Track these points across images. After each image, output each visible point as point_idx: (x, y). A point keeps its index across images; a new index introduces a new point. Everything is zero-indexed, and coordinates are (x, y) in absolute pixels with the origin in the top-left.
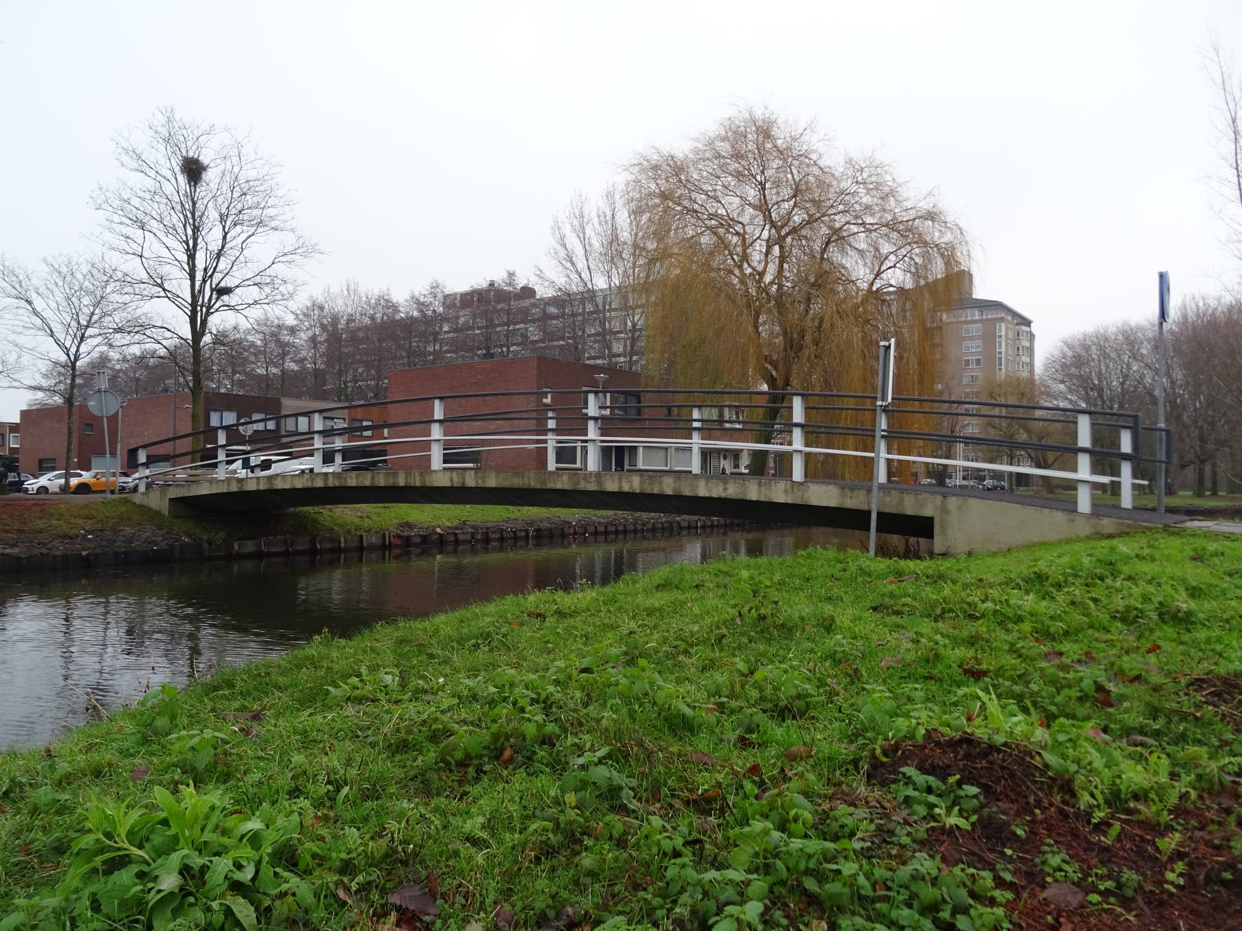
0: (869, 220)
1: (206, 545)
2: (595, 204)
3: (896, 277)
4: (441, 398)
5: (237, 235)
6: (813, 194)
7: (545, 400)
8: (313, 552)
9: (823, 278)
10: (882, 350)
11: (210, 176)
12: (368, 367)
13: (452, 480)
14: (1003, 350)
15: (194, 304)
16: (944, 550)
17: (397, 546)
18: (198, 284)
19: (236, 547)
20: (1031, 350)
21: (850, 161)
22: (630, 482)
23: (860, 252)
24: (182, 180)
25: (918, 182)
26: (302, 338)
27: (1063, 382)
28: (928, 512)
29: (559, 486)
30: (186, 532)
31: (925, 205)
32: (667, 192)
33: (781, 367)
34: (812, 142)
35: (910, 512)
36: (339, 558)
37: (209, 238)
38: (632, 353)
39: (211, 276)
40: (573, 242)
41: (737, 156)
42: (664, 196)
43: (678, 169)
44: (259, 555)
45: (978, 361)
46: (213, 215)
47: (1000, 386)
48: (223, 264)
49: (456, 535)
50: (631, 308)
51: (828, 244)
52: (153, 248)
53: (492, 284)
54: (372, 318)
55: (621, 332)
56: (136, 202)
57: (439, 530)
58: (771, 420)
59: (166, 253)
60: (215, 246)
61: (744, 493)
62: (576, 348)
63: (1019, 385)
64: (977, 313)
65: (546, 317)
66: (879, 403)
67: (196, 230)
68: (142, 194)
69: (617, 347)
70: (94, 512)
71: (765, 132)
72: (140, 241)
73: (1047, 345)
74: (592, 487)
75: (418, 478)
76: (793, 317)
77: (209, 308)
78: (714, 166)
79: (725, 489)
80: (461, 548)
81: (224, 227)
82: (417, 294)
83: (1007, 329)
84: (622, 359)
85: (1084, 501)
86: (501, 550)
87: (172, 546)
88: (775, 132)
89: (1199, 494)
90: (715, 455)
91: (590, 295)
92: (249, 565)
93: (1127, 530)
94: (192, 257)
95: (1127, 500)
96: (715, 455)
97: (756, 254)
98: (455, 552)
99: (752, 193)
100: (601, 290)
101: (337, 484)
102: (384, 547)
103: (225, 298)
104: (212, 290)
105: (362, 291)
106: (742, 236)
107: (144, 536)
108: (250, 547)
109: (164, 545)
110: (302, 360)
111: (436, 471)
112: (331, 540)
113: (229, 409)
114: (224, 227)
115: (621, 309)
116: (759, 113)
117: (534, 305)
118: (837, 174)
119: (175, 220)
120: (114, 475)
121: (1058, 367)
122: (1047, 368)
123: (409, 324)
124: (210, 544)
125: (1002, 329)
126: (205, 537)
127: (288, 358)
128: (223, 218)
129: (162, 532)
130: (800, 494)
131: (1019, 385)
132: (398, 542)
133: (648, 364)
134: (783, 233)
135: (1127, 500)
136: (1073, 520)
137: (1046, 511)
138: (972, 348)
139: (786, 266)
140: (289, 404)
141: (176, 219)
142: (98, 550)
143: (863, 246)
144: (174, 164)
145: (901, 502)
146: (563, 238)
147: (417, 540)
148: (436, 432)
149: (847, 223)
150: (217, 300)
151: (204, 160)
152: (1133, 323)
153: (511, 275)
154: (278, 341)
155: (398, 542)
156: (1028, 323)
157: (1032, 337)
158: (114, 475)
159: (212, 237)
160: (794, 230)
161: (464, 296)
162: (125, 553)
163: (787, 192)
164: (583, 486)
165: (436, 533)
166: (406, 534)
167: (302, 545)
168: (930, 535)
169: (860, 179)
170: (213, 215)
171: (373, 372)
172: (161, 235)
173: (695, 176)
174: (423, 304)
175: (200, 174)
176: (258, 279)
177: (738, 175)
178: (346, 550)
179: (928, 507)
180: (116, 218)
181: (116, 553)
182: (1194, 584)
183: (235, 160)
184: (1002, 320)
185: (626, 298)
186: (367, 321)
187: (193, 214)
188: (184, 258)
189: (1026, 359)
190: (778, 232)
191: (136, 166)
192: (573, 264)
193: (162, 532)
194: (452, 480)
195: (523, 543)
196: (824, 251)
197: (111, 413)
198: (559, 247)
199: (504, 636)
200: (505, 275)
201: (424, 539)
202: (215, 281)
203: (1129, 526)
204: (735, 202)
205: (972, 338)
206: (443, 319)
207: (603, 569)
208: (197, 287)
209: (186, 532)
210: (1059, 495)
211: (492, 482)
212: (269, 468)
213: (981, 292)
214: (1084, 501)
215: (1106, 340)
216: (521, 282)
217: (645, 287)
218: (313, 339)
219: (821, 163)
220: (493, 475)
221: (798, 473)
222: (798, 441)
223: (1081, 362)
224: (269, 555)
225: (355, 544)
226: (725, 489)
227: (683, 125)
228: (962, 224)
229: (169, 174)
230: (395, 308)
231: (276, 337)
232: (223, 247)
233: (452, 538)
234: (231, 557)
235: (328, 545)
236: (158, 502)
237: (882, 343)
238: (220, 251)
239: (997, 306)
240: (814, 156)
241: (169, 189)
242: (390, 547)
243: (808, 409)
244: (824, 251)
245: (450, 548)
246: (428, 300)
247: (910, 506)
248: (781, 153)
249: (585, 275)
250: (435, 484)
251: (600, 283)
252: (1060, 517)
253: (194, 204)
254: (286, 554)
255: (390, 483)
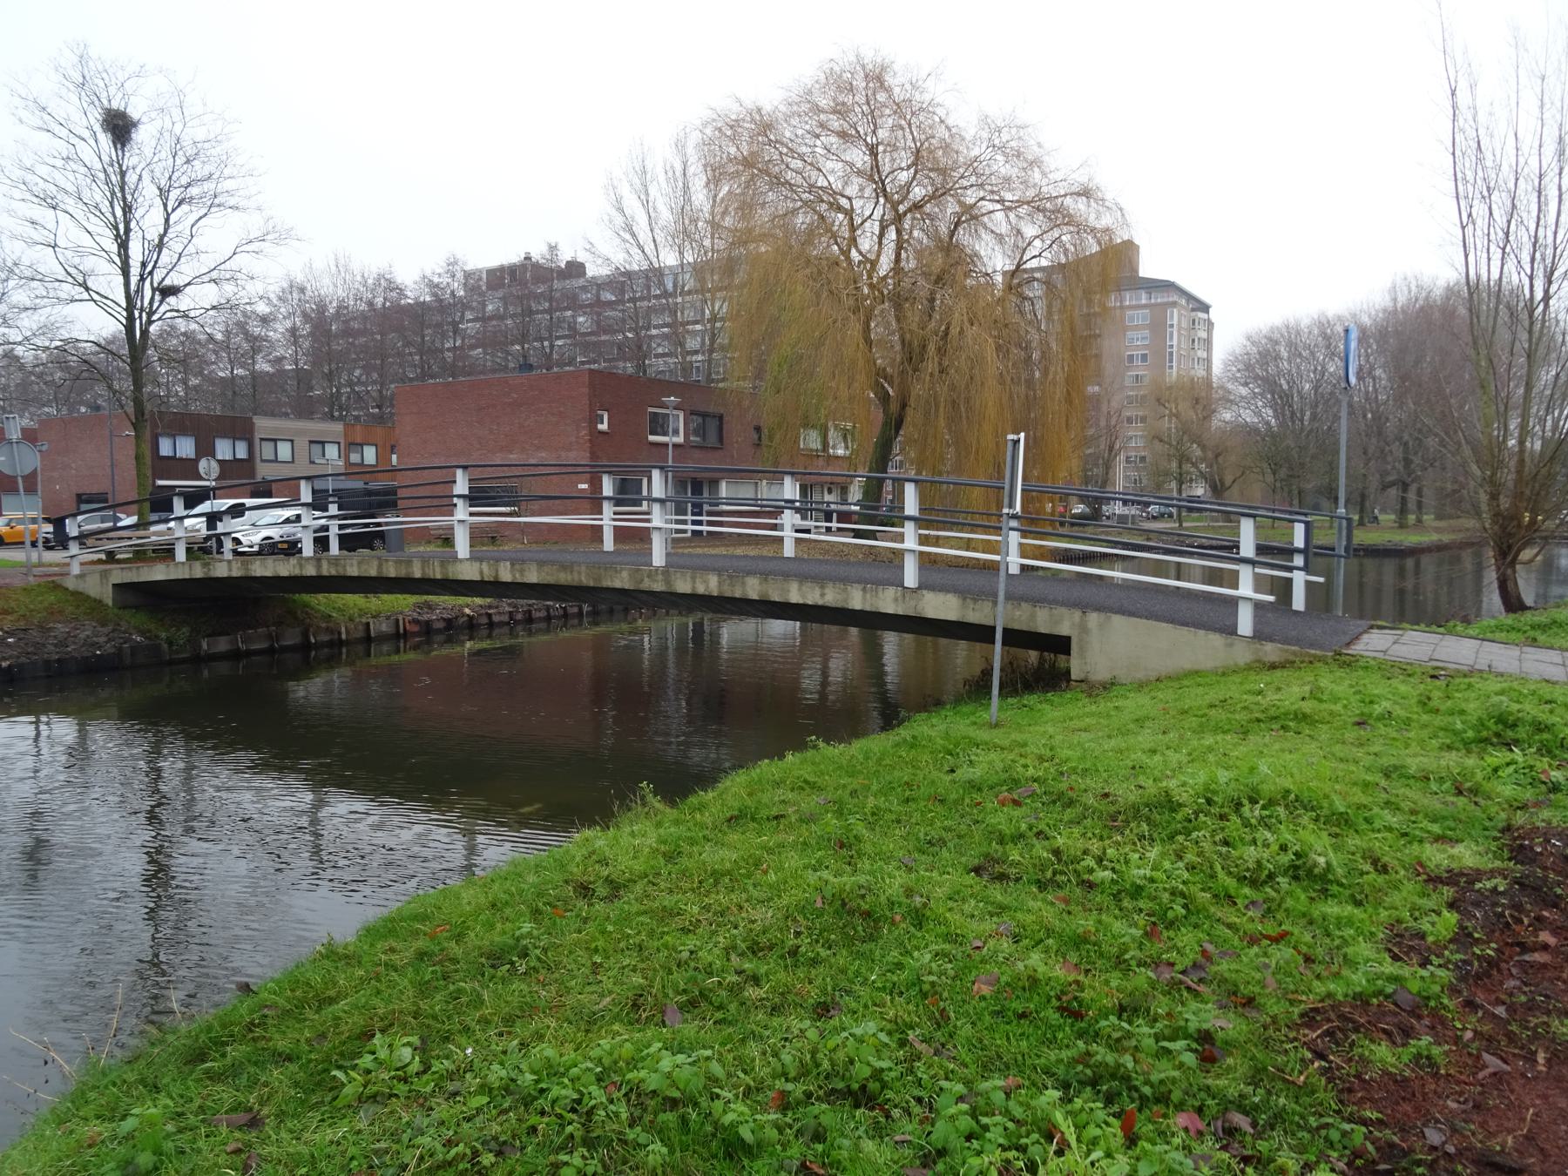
0: (1008, 196)
1: (165, 646)
2: (662, 157)
3: (1040, 258)
4: (465, 468)
5: (183, 217)
6: (935, 161)
7: (600, 427)
8: (305, 647)
9: (950, 262)
10: (1010, 445)
11: (140, 136)
12: (367, 369)
13: (481, 573)
14: (1175, 343)
15: (130, 308)
16: (1082, 676)
17: (415, 634)
18: (134, 280)
19: (205, 646)
20: (1208, 343)
21: (985, 120)
22: (706, 582)
23: (1000, 238)
24: (105, 140)
25: (1066, 159)
26: (277, 332)
27: (1246, 384)
28: (1064, 629)
29: (618, 584)
30: (136, 630)
31: (1081, 178)
32: (749, 158)
33: (896, 381)
34: (934, 91)
35: (1042, 630)
36: (340, 653)
37: (145, 224)
38: (711, 351)
39: (151, 273)
40: (633, 206)
41: (840, 110)
42: (748, 162)
43: (765, 127)
44: (235, 655)
45: (1144, 357)
46: (149, 191)
47: (1170, 388)
48: (166, 258)
49: (489, 616)
50: (709, 291)
51: (957, 225)
52: (70, 234)
53: (528, 258)
54: (370, 304)
55: (696, 322)
56: (43, 170)
57: (467, 611)
58: (879, 512)
59: (87, 241)
60: (153, 235)
61: (846, 600)
62: (640, 347)
63: (1193, 388)
64: (1144, 296)
65: (599, 303)
66: (1005, 511)
67: (127, 209)
68: (52, 161)
69: (692, 343)
70: (13, 604)
71: (877, 78)
72: (51, 226)
73: (1231, 334)
74: (658, 587)
75: (438, 569)
76: (913, 316)
77: (151, 313)
78: (812, 124)
79: (823, 595)
80: (496, 631)
81: (165, 205)
82: (428, 273)
83: (1180, 315)
84: (700, 358)
85: (1245, 622)
86: (548, 631)
87: (120, 649)
88: (889, 80)
89: (1402, 525)
90: (818, 488)
91: (654, 274)
92: (223, 668)
93: (1292, 658)
94: (123, 245)
95: (1299, 602)
96: (818, 488)
97: (866, 243)
98: (490, 636)
99: (859, 157)
100: (670, 268)
101: (333, 573)
102: (398, 637)
103: (172, 300)
104: (154, 290)
105: (356, 267)
106: (849, 213)
107: (82, 636)
108: (223, 645)
109: (109, 648)
110: (280, 360)
111: (461, 561)
112: (329, 630)
113: (184, 432)
114: (165, 205)
115: (697, 292)
116: (868, 57)
117: (583, 288)
118: (968, 137)
119: (98, 197)
120: (34, 521)
121: (1241, 366)
122: (1227, 365)
123: (418, 312)
124: (170, 644)
125: (1175, 317)
126: (163, 635)
127: (259, 358)
128: (163, 193)
129: (105, 630)
130: (913, 603)
131: (1193, 388)
132: (416, 628)
133: (734, 379)
134: (901, 208)
135: (1299, 602)
136: (1231, 645)
137: (1202, 632)
138: (1138, 340)
139: (903, 255)
140: (263, 425)
141: (99, 196)
142: (23, 660)
143: (1003, 229)
144: (93, 121)
145: (1033, 616)
146: (619, 200)
147: (441, 625)
148: (462, 512)
149: (982, 199)
150: (161, 302)
151: (134, 114)
152: (1331, 314)
153: (553, 248)
154: (246, 333)
155: (416, 628)
156: (1205, 308)
157: (1210, 325)
158: (34, 521)
159: (149, 220)
160: (917, 206)
161: (490, 272)
162: (59, 661)
163: (905, 158)
164: (647, 585)
165: (464, 615)
166: (426, 617)
167: (291, 638)
168: (1067, 652)
169: (997, 142)
170: (149, 191)
171: (375, 376)
172: (79, 215)
173: (788, 134)
174: (437, 286)
175: (129, 132)
176: (214, 275)
177: (842, 135)
178: (347, 643)
179: (1062, 623)
180: (17, 194)
181: (47, 662)
182: (1342, 809)
183: (176, 113)
184: (1174, 304)
185: (702, 281)
186: (363, 307)
187: (122, 190)
188: (114, 248)
189: (1202, 354)
190: (895, 207)
191: (40, 123)
192: (633, 235)
193: (105, 630)
194: (481, 573)
195: (576, 621)
196: (952, 234)
197: (27, 471)
198: (614, 213)
199: (545, 950)
200: (545, 249)
201: (449, 623)
202: (157, 277)
203: (1294, 653)
204: (837, 168)
205: (1137, 328)
206: (463, 305)
207: (677, 649)
208: (133, 287)
209: (136, 630)
210: (1215, 615)
211: (532, 577)
212: (241, 514)
213: (1148, 268)
214: (1245, 622)
215: (1298, 333)
216: (565, 256)
217: (729, 266)
218: (293, 331)
219: (950, 122)
220: (534, 567)
221: (911, 577)
222: (910, 539)
223: (1267, 363)
224: (249, 653)
225: (360, 634)
226: (823, 595)
227: (772, 73)
228: (1119, 200)
229: (87, 134)
230: (401, 291)
231: (244, 334)
232: (166, 231)
233: (485, 620)
234: (199, 659)
235: (325, 638)
236: (100, 589)
237: (1011, 437)
238: (162, 237)
239: (1168, 286)
240: (941, 112)
241: (88, 154)
242: (406, 635)
243: (922, 498)
244: (952, 234)
245: (485, 632)
246: (446, 280)
247: (1043, 621)
248: (898, 109)
249: (649, 248)
250: (461, 577)
251: (669, 259)
252: (1216, 640)
253: (123, 174)
254: (271, 651)
255: (403, 573)
